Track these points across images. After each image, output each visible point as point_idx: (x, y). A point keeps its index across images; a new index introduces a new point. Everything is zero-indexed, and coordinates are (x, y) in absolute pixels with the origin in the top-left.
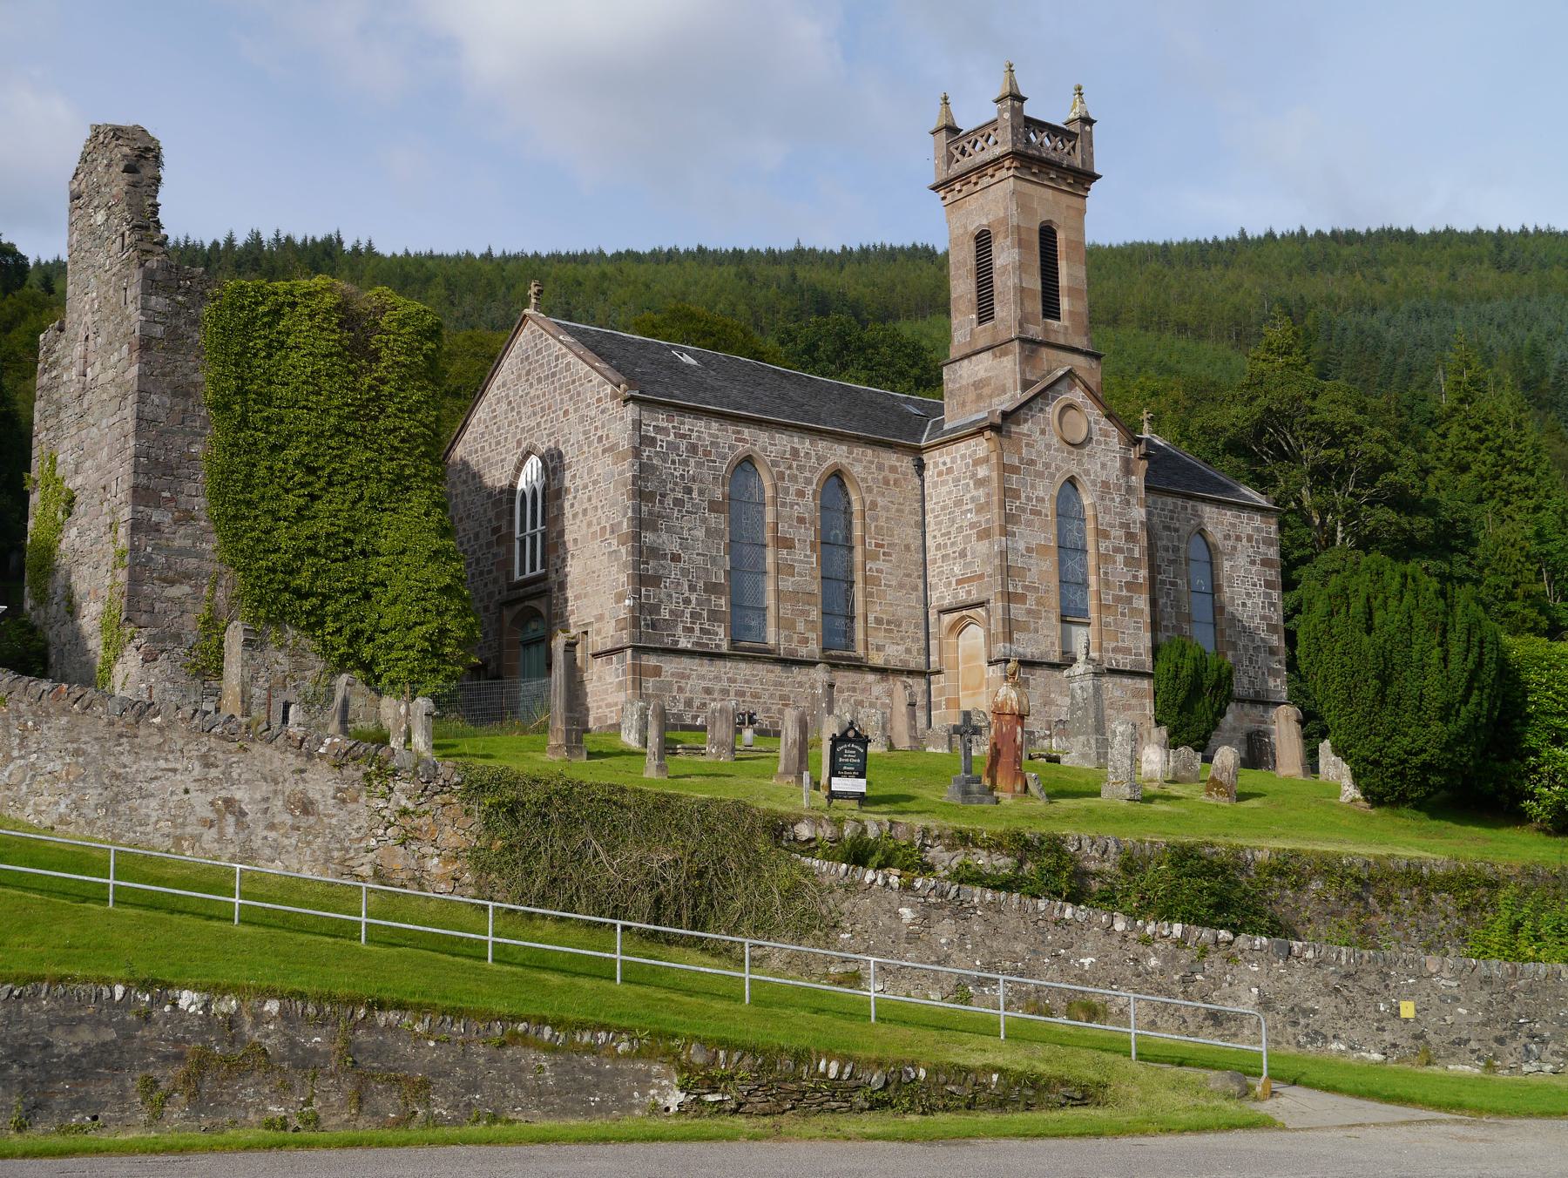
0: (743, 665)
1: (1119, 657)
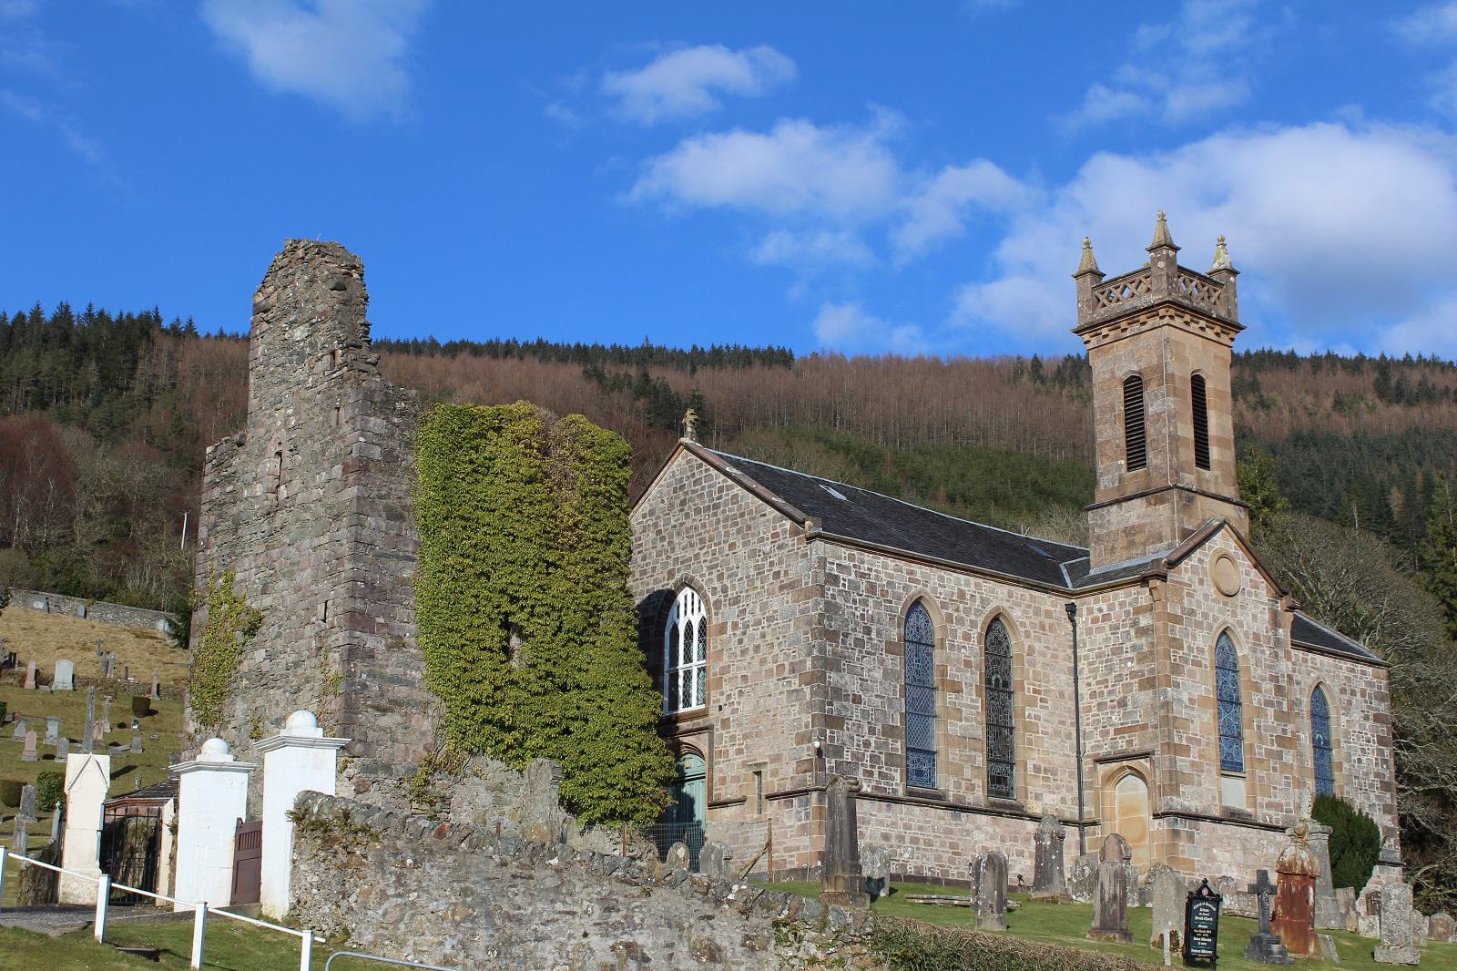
0: (917, 810)
1: (1272, 812)
